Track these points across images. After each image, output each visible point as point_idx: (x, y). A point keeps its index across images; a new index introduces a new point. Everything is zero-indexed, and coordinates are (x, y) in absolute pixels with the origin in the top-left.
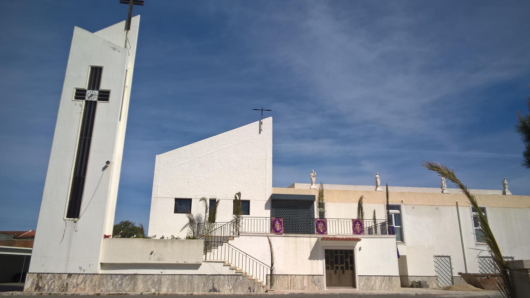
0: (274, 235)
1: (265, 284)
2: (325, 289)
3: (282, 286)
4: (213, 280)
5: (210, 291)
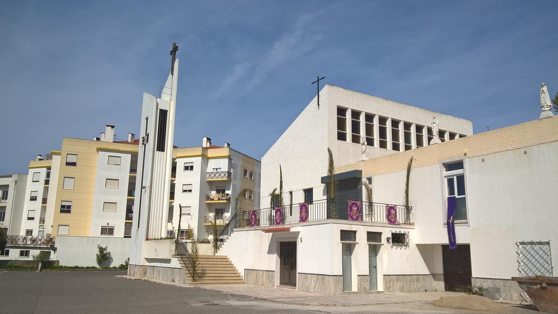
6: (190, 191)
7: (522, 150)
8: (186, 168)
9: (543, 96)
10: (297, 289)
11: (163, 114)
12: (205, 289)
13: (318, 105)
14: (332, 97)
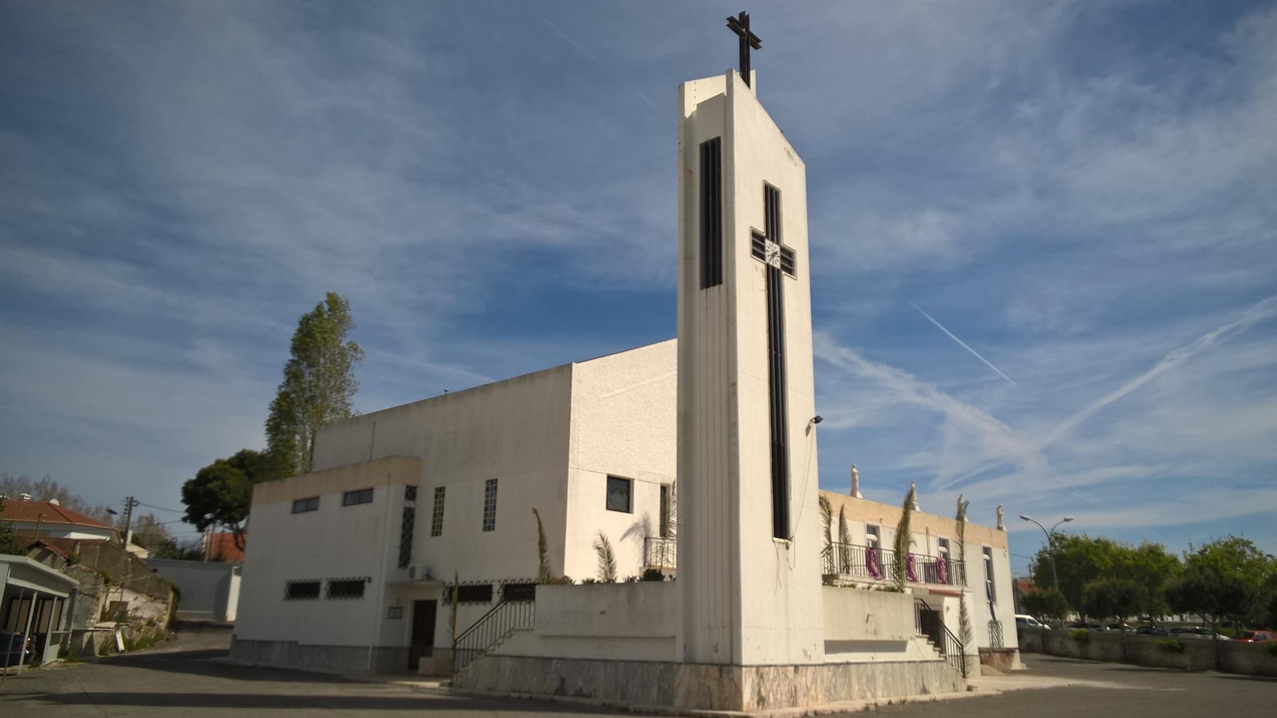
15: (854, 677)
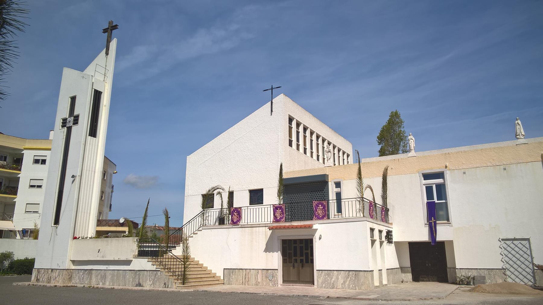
0: (231, 226)
1: (222, 278)
2: (279, 286)
3: (237, 281)
4: (139, 275)
5: (137, 286)
6: (40, 187)
7: (502, 167)
8: (36, 161)
9: (518, 127)
10: (315, 286)
11: (97, 95)
12: (219, 293)
13: (272, 111)
14: (283, 104)
15: (93, 276)
